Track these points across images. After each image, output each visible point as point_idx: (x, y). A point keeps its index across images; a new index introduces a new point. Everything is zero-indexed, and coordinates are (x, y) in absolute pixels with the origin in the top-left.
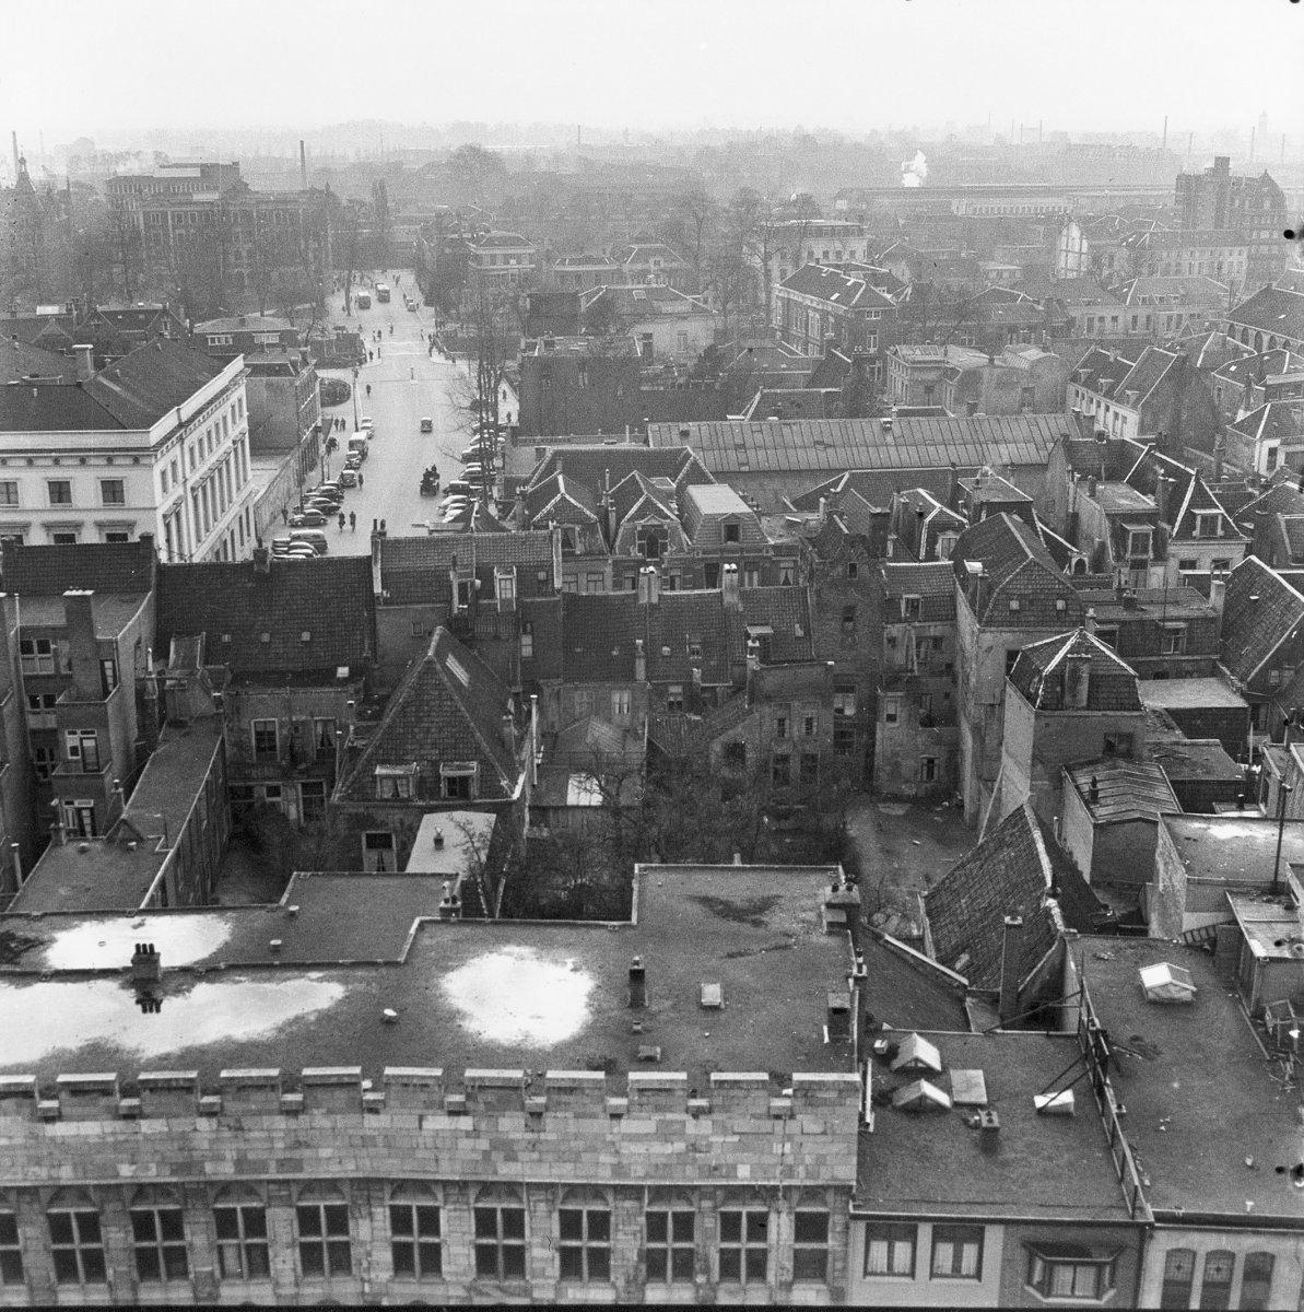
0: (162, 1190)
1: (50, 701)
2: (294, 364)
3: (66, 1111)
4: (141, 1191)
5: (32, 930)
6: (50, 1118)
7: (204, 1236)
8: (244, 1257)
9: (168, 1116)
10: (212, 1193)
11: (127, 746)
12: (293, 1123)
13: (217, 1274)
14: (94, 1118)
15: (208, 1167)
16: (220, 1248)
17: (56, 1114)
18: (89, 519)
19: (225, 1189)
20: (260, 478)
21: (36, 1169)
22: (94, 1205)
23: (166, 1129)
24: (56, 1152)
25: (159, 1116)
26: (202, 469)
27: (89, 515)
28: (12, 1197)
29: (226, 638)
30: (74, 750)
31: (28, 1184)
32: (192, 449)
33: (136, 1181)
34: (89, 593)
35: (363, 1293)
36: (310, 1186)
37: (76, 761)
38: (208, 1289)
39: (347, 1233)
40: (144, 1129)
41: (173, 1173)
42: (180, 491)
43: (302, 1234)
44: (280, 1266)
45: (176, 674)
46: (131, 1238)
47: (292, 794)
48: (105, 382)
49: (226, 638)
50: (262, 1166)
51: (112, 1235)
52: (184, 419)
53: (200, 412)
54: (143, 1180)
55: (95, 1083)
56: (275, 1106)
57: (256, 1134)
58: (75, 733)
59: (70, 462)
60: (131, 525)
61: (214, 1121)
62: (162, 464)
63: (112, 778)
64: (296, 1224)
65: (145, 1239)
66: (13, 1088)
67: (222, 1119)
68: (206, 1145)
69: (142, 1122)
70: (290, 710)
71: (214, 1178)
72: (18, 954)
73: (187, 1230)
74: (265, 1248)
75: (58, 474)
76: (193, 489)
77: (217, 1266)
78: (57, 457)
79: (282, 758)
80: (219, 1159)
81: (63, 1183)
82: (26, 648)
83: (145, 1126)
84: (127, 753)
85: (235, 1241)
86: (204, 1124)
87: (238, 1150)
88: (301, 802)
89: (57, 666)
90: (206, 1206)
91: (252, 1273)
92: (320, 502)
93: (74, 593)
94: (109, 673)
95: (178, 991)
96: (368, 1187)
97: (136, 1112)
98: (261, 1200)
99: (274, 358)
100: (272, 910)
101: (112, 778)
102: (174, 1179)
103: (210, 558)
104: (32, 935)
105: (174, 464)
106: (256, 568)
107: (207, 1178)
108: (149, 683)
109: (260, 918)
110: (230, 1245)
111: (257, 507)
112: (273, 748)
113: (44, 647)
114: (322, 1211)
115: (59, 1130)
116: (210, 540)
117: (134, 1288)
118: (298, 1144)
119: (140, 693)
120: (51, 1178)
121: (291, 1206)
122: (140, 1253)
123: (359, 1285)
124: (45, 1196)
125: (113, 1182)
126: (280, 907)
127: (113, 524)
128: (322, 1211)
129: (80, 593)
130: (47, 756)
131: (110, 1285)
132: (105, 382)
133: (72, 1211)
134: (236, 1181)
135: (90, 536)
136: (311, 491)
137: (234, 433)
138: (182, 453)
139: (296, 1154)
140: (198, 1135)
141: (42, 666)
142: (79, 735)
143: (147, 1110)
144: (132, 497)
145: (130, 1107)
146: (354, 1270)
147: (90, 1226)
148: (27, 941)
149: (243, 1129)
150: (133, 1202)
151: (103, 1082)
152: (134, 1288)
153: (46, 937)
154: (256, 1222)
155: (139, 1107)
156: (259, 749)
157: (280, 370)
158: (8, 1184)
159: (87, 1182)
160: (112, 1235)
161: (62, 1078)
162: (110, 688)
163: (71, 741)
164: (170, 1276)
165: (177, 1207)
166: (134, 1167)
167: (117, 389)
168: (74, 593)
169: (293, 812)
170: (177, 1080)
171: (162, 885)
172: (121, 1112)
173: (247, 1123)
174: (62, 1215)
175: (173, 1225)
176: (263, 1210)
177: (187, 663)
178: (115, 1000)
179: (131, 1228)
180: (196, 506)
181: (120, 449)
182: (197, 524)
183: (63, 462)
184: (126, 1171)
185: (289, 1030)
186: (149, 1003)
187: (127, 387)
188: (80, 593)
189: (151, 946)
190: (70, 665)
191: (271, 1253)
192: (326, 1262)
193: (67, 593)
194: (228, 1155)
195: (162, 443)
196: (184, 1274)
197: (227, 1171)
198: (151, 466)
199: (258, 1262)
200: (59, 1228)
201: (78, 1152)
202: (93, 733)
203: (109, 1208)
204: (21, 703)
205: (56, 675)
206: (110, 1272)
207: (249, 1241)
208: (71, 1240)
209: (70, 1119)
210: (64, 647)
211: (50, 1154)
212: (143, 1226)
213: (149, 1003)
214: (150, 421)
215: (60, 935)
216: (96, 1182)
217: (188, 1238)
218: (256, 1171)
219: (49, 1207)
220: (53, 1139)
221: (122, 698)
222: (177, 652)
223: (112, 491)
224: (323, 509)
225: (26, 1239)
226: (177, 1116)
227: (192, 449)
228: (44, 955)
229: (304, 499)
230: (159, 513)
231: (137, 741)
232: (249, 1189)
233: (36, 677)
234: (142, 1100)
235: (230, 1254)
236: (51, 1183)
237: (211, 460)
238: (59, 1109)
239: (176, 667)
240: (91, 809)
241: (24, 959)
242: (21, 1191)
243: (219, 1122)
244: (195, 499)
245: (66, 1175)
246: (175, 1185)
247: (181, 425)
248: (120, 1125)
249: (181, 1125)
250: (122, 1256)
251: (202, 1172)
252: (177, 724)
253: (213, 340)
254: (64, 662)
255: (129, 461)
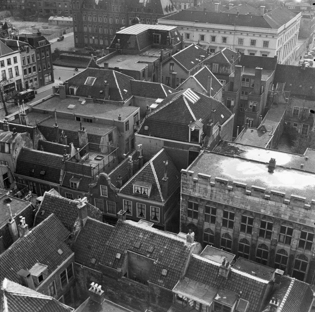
0: (270, 218)
1: (246, 93)
2: (312, 15)
3: (252, 194)
4: (265, 217)
5: (243, 148)
6: (248, 194)
7: (277, 231)
8: (285, 239)
9: (276, 201)
10: (281, 222)
11: (263, 107)
12: (306, 211)
13: (278, 240)
14: (258, 197)
15: (282, 216)
16: (280, 235)
17: (250, 194)
18: (259, 50)
19: (285, 222)
20: (299, 45)
21: (242, 205)
22: (253, 217)
23: (274, 204)
24: (248, 202)
25: (274, 201)
26: (287, 41)
27: (259, 50)
28: (235, 209)
29: (291, 85)
30: (251, 106)
31: (239, 208)
32: (286, 35)
33: (264, 214)
34: (262, 69)
35: (312, 256)
36: (306, 227)
37: (251, 109)
38: (275, 243)
39: (271, 230)
40: (269, 203)
41: (273, 215)
42: (281, 46)
43: (301, 238)
44: (293, 243)
45: (277, 92)
46: (260, 227)
47: (300, 126)
48: (268, 16)
49: (291, 85)
50: (296, 219)
51: (255, 224)
52: (286, 27)
53: (290, 26)
54: (266, 214)
55: (261, 189)
56: (303, 206)
57: (297, 212)
58: (252, 102)
59: (239, 34)
60: (269, 53)
61: (287, 206)
62: (279, 38)
63: (259, 113)
64: (300, 235)
65: (244, 223)
66: (241, 186)
67: (289, 206)
68: (283, 211)
69: (269, 201)
70: (304, 106)
71: (283, 219)
72: (239, 153)
73: (273, 228)
74: (291, 238)
75: (266, 39)
76: (284, 46)
77: (278, 239)
78: (254, 34)
79: (299, 117)
80: (285, 214)
81: (247, 210)
82: (243, 80)
83: (270, 202)
84: (263, 109)
85: (284, 235)
86: (284, 206)
87: (291, 214)
88: (302, 129)
89: (250, 85)
90: (279, 225)
91: (286, 243)
92: (312, 53)
93: (258, 68)
94: (262, 89)
95: (277, 170)
96: (239, 210)
97: (269, 198)
98: (293, 227)
99: (307, 14)
100: (301, 156)
101: (259, 113)
102: (273, 216)
103: (284, 64)
104: (243, 149)
105: (281, 38)
106: (302, 68)
107: (281, 218)
108: (272, 94)
109: (298, 157)
110: (282, 235)
111: (297, 52)
112: (298, 114)
113: (248, 80)
114: (308, 233)
115: (250, 198)
116: (285, 59)
117: (257, 237)
118: (306, 217)
119: (269, 95)
120: (245, 208)
121: (300, 231)
122: (242, 225)
123: (312, 253)
124: (242, 212)
125: (259, 213)
126: (303, 156)
127: (264, 52)
128: (308, 233)
129: (259, 68)
130: (243, 106)
131: (252, 235)
132: (268, 16)
133: (248, 216)
134: (288, 221)
135: (258, 54)
136: (310, 49)
137: (295, 32)
138: (284, 36)
139: (305, 219)
140: (281, 208)
141: (246, 85)
142: (253, 103)
143: (271, 199)
144: (270, 46)
145: (267, 197)
146: (312, 250)
147: (251, 221)
148: (242, 150)
149: (293, 209)
150: (262, 219)
151: (262, 190)
152: (257, 237)
153: (246, 151)
154: (290, 231)
155: (270, 198)
156: (294, 114)
157: (308, 17)
158: (235, 207)
159: (253, 211)
160: (255, 224)
161: (253, 186)
162: (262, 93)
163: (251, 104)
164: (266, 238)
165: (272, 223)
166: (264, 211)
167: (271, 18)
168: (258, 68)
169: (299, 131)
170: (280, 194)
171: (270, 143)
172: (265, 197)
173: (294, 208)
174: (245, 217)
175: (270, 226)
176: (292, 229)
177: (280, 89)
178: (264, 169)
179: (260, 224)
180: (284, 50)
181: (257, 32)
182: (284, 54)
183: (268, 37)
184: (262, 211)
185: (307, 188)
186: (271, 171)
187: (272, 17)
188: (259, 68)
189: (275, 159)
190: (253, 86)
191: (292, 239)
192: (305, 246)
193: (256, 68)
194: (288, 214)
195: (280, 33)
196: (270, 238)
197: (287, 218)
198: (276, 39)
199: (288, 241)
200: (244, 219)
201: (253, 204)
202: (256, 103)
203: (257, 218)
204: (240, 92)
205: (249, 88)
206: (253, 233)
207: (288, 235)
208: (246, 223)
209: (253, 196)
210: (252, 81)
211: (246, 202)
212: (263, 225)
213: (271, 171)
214: (278, 27)
215: (249, 150)
216: (255, 212)
217: (273, 230)
218: (294, 220)
219: (243, 214)
220: (247, 199)
221: (264, 95)
222: (278, 86)
223: (266, 44)
224: (313, 54)
225: (236, 220)
226: (278, 202)
227: (286, 35)
228: (245, 155)
229: (308, 51)
230: (276, 50)
231: (265, 106)
232: (291, 224)
233: (245, 87)
234: (271, 196)
235: (282, 237)
236: (245, 209)
237: (290, 38)
238: (290, 202)
239: (277, 90)
240: (252, 121)
241: (241, 154)
242: (237, 209)
243: (288, 206)
244: (284, 48)
245: (248, 208)
246: (273, 217)
247: (285, 29)
248: (264, 200)
249: (278, 204)
250: (257, 230)
251: (281, 217)
252: (275, 104)
253: (290, 8)
254: (251, 84)
255: (258, 36)
